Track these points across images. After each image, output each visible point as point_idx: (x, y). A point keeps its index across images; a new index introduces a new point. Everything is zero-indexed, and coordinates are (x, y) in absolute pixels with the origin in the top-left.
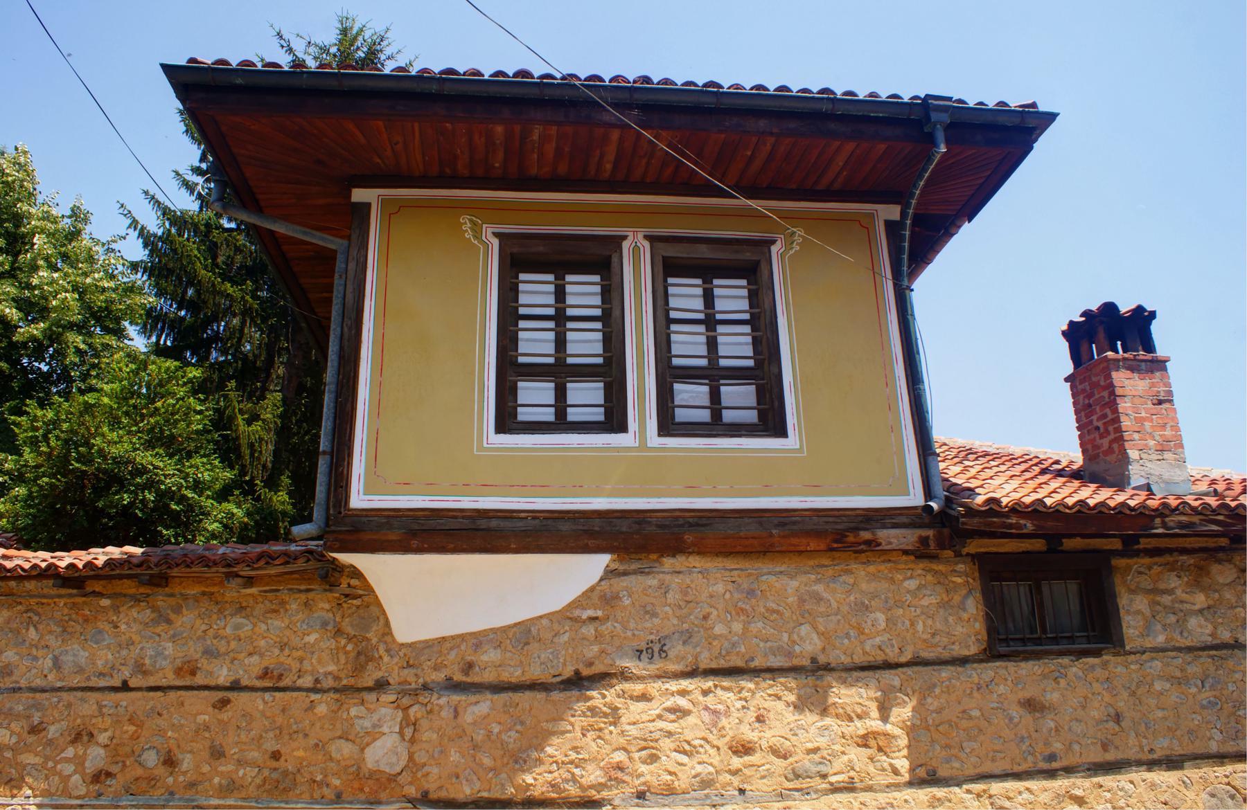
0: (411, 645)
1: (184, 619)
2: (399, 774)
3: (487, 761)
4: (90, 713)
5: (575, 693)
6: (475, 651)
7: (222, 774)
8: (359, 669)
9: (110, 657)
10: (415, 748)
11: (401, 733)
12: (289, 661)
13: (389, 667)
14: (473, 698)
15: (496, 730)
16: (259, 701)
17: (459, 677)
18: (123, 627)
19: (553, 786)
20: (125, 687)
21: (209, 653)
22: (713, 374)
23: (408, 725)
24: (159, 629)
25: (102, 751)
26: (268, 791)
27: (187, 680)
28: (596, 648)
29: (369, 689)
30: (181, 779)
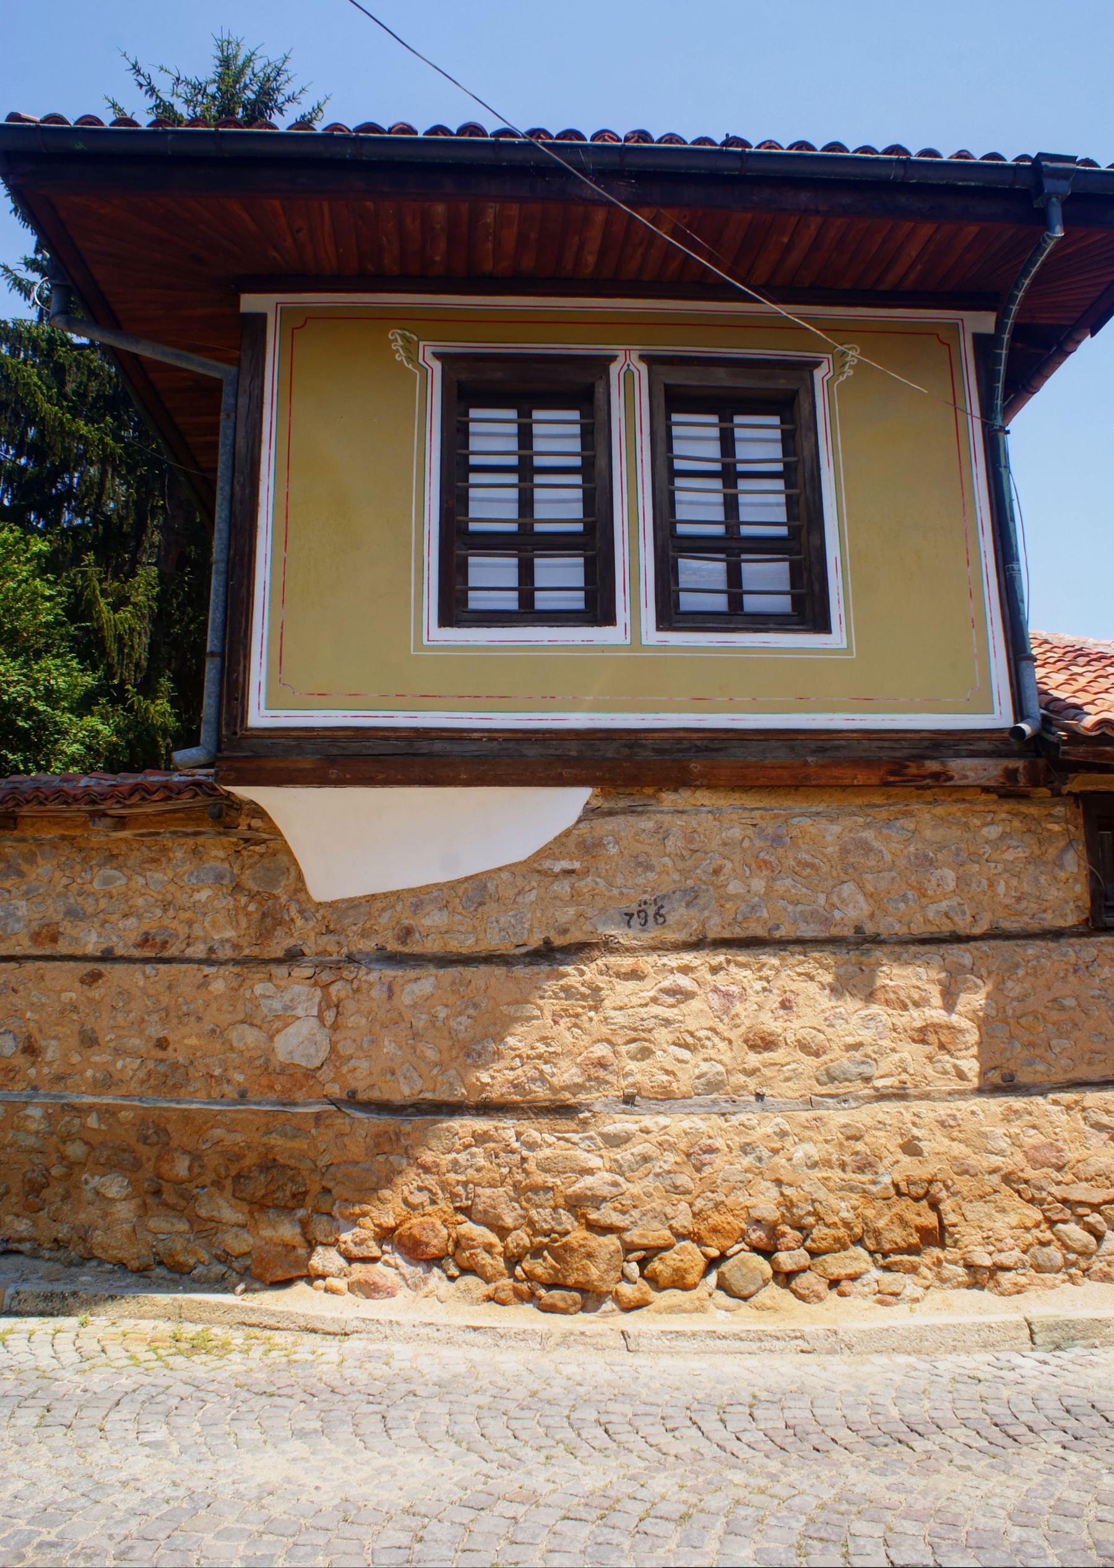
0: (331, 905)
1: (40, 870)
2: (319, 1068)
5: (545, 968)
6: (415, 913)
8: (264, 936)
11: (320, 1017)
12: (175, 924)
13: (303, 933)
14: (412, 974)
17: (393, 946)
19: (515, 1086)
22: (732, 546)
23: (329, 1007)
28: (572, 911)
29: (279, 961)
30: (46, 1070)
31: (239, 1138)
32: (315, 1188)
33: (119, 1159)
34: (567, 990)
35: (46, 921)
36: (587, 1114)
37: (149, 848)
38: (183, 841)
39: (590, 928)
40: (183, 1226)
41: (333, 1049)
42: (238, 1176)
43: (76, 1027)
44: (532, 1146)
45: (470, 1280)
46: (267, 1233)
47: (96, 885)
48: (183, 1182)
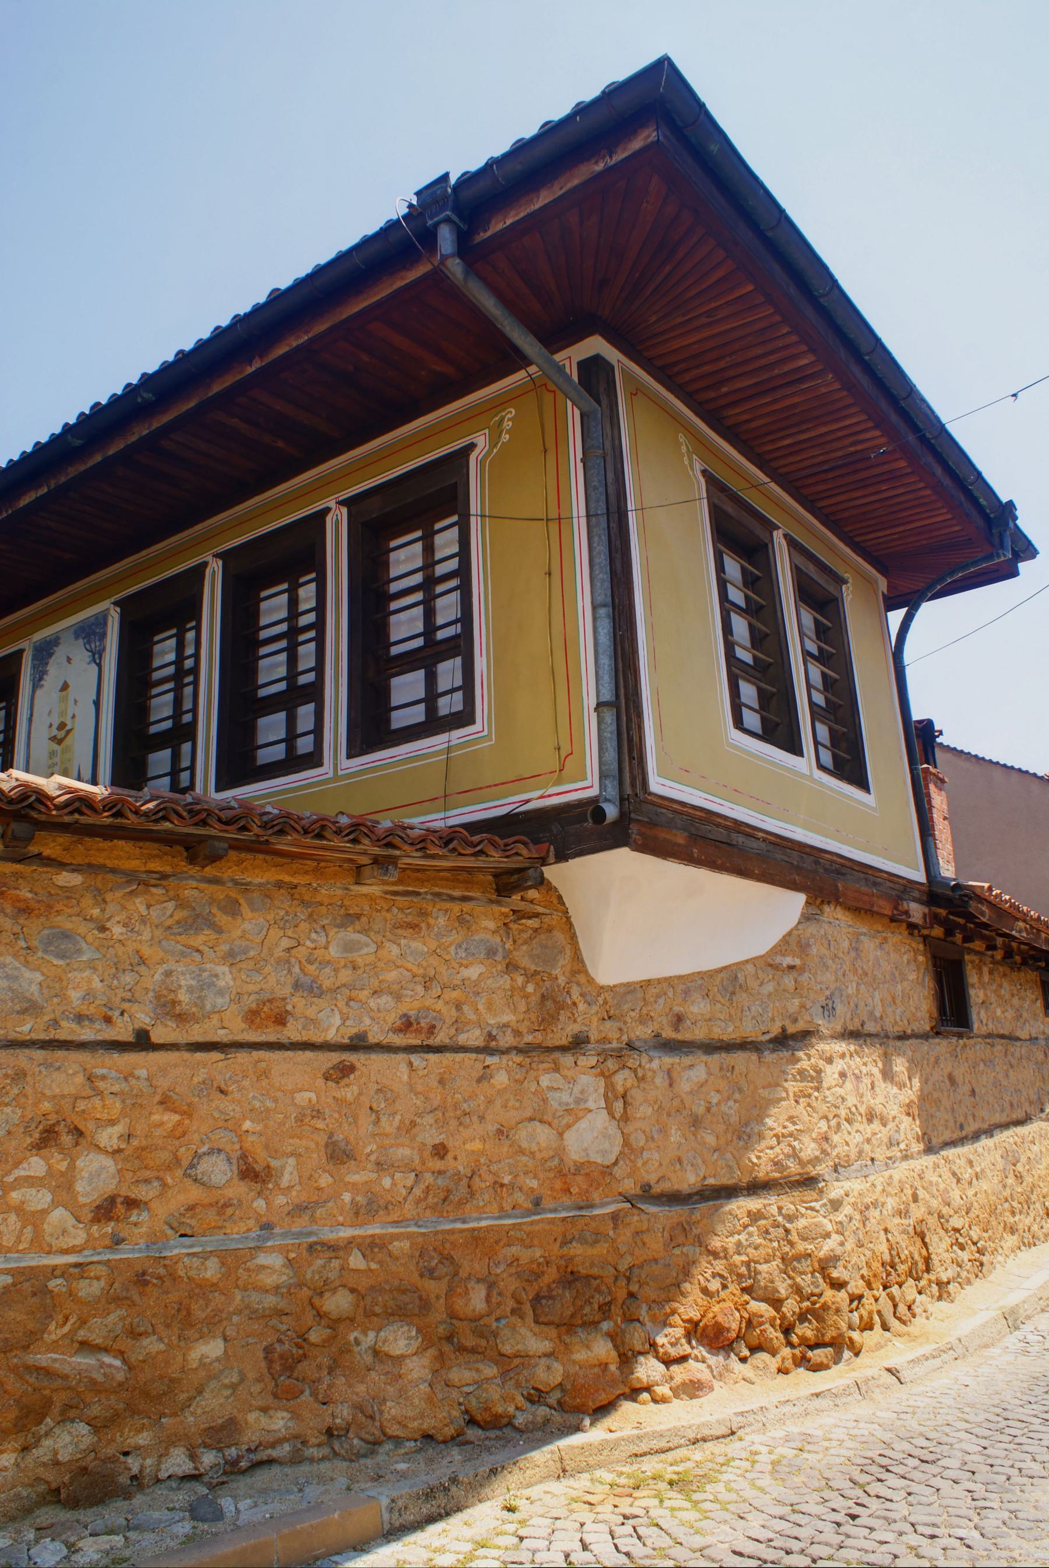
0: (611, 988)
1: (247, 926)
2: (615, 1163)
3: (711, 1140)
4: (69, 1089)
5: (786, 1054)
6: (684, 1000)
7: (354, 1187)
8: (547, 1021)
9: (96, 984)
10: (629, 1128)
11: (609, 1109)
12: (440, 1005)
13: (584, 1019)
14: (687, 1060)
15: (715, 1101)
16: (404, 1068)
17: (668, 1033)
18: (117, 930)
19: (776, 1164)
20: (142, 1042)
21: (313, 990)
23: (616, 1098)
24: (198, 941)
25: (108, 1162)
26: (433, 1208)
27: (269, 1032)
28: (796, 1002)
29: (563, 1049)
30: (281, 1200)
31: (538, 1253)
32: (622, 1294)
33: (404, 1306)
34: (801, 1072)
35: (268, 996)
36: (823, 1184)
37: (400, 909)
38: (448, 905)
39: (808, 1018)
40: (490, 1371)
41: (626, 1143)
42: (537, 1299)
43: (322, 1139)
44: (790, 1218)
45: (764, 1356)
46: (580, 1355)
47: (334, 952)
48: (481, 1317)
